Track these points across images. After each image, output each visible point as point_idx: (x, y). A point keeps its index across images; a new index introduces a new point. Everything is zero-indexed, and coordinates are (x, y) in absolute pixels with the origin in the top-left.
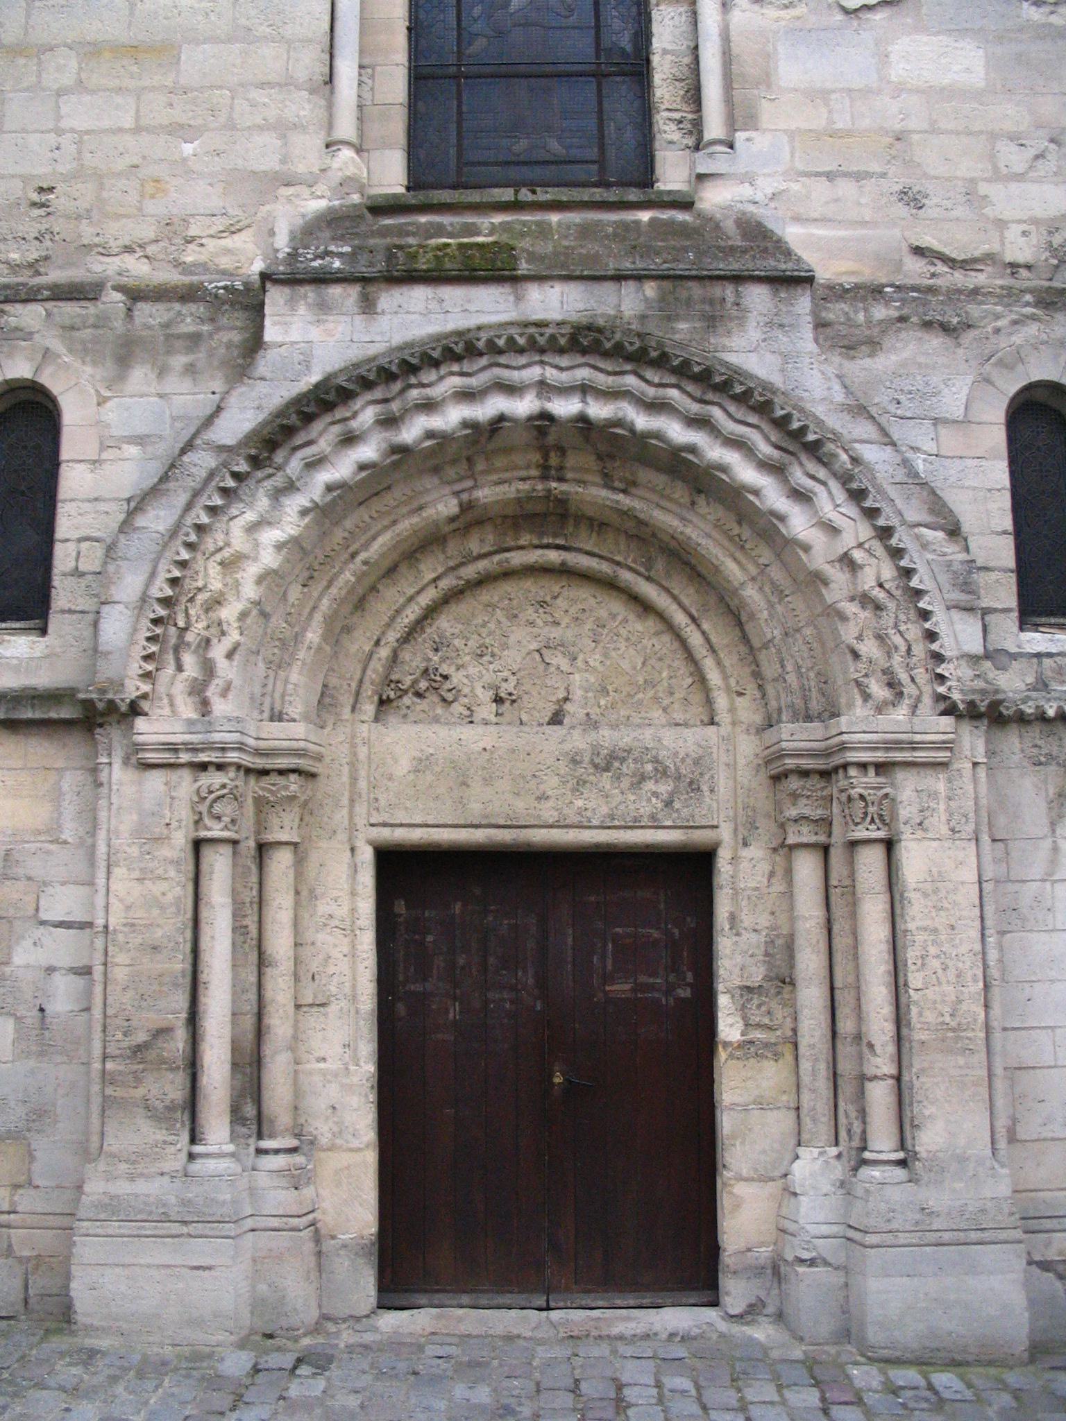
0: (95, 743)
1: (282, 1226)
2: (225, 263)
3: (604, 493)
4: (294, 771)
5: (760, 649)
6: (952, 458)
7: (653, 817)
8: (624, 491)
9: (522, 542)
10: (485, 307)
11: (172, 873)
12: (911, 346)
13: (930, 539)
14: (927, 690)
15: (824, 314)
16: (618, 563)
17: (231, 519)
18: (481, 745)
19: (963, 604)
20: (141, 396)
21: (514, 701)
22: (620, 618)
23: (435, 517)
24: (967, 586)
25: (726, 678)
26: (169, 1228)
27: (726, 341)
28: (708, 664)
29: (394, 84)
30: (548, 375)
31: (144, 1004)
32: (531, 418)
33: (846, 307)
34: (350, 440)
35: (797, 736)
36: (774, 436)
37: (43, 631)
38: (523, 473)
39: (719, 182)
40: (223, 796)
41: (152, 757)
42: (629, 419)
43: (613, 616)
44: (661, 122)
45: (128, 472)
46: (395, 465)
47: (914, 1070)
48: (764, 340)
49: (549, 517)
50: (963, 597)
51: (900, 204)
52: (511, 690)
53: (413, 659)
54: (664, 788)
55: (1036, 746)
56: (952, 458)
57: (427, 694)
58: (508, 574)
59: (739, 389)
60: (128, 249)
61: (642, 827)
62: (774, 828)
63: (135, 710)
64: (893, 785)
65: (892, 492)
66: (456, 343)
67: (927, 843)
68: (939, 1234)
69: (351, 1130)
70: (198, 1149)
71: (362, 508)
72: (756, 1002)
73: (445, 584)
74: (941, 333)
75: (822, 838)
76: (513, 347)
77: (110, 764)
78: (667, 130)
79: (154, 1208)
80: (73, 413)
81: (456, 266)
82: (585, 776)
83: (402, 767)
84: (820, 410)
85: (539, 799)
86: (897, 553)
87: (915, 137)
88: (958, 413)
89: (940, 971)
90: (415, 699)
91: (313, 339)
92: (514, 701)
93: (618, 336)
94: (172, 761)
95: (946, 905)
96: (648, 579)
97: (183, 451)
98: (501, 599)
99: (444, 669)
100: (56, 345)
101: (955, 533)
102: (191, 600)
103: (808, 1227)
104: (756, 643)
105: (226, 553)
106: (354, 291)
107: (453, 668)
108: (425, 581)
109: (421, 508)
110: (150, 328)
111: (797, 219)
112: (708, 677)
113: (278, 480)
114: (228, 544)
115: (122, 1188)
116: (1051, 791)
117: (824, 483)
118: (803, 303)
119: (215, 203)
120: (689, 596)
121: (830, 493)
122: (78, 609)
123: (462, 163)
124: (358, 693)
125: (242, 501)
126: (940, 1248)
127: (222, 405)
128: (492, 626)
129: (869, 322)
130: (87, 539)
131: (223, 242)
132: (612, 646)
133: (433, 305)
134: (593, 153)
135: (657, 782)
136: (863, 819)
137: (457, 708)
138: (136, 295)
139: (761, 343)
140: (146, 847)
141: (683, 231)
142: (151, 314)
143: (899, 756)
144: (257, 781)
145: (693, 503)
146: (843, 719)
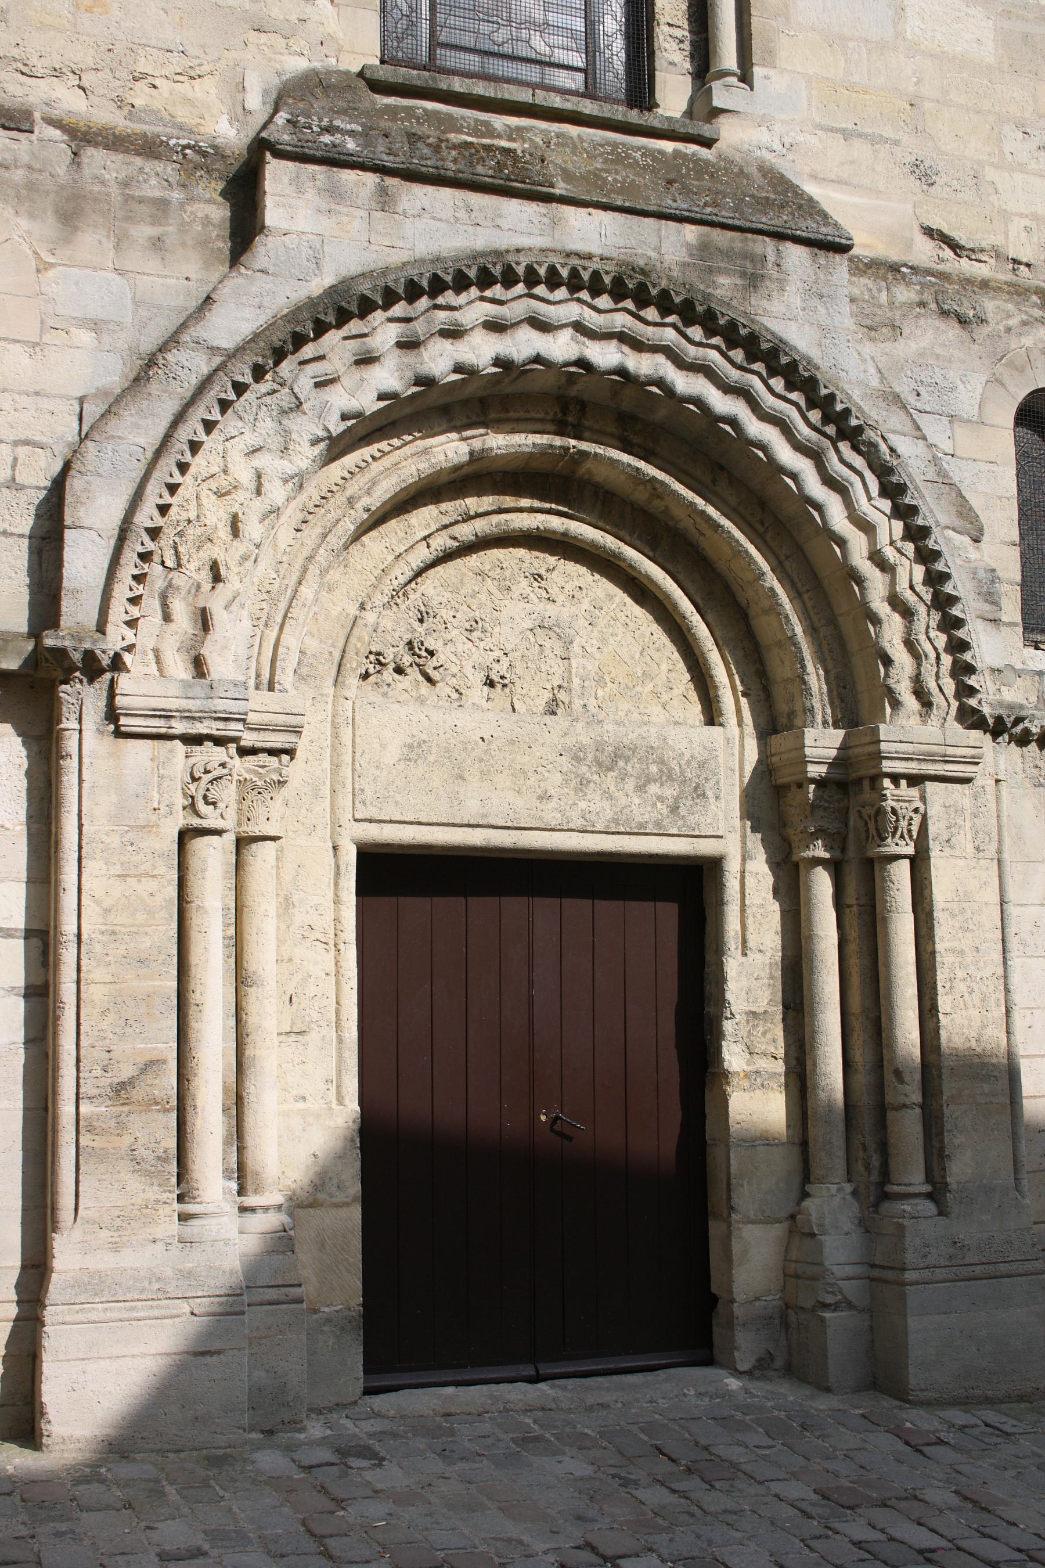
1: (283, 1298)
2: (184, 115)
6: (967, 459)
7: (658, 824)
10: (515, 226)
11: (162, 870)
13: (957, 543)
20: (95, 269)
21: (504, 686)
26: (168, 1307)
27: (765, 304)
30: (586, 316)
31: (128, 1030)
33: (870, 283)
34: (366, 360)
44: (661, 38)
47: (945, 1098)
50: (987, 607)
51: (912, 178)
53: (393, 628)
54: (670, 792)
56: (967, 459)
57: (409, 670)
59: (784, 360)
60: (57, 73)
67: (952, 860)
68: (971, 1268)
69: (335, 1182)
70: (190, 1208)
72: (761, 1029)
74: (957, 325)
76: (553, 281)
79: (146, 1284)
81: (490, 172)
82: (588, 775)
83: (393, 752)
84: (856, 394)
85: (540, 798)
89: (966, 995)
90: (396, 676)
91: (322, 228)
92: (504, 686)
93: (664, 283)
94: (163, 731)
103: (835, 1269)
106: (370, 179)
107: (440, 643)
111: (814, 177)
115: (104, 1261)
122: (16, 531)
126: (972, 1282)
127: (214, 296)
128: (483, 597)
130: (27, 443)
132: (611, 630)
133: (462, 214)
135: (662, 785)
138: (81, 137)
139: (799, 307)
140: (129, 836)
141: (701, 167)
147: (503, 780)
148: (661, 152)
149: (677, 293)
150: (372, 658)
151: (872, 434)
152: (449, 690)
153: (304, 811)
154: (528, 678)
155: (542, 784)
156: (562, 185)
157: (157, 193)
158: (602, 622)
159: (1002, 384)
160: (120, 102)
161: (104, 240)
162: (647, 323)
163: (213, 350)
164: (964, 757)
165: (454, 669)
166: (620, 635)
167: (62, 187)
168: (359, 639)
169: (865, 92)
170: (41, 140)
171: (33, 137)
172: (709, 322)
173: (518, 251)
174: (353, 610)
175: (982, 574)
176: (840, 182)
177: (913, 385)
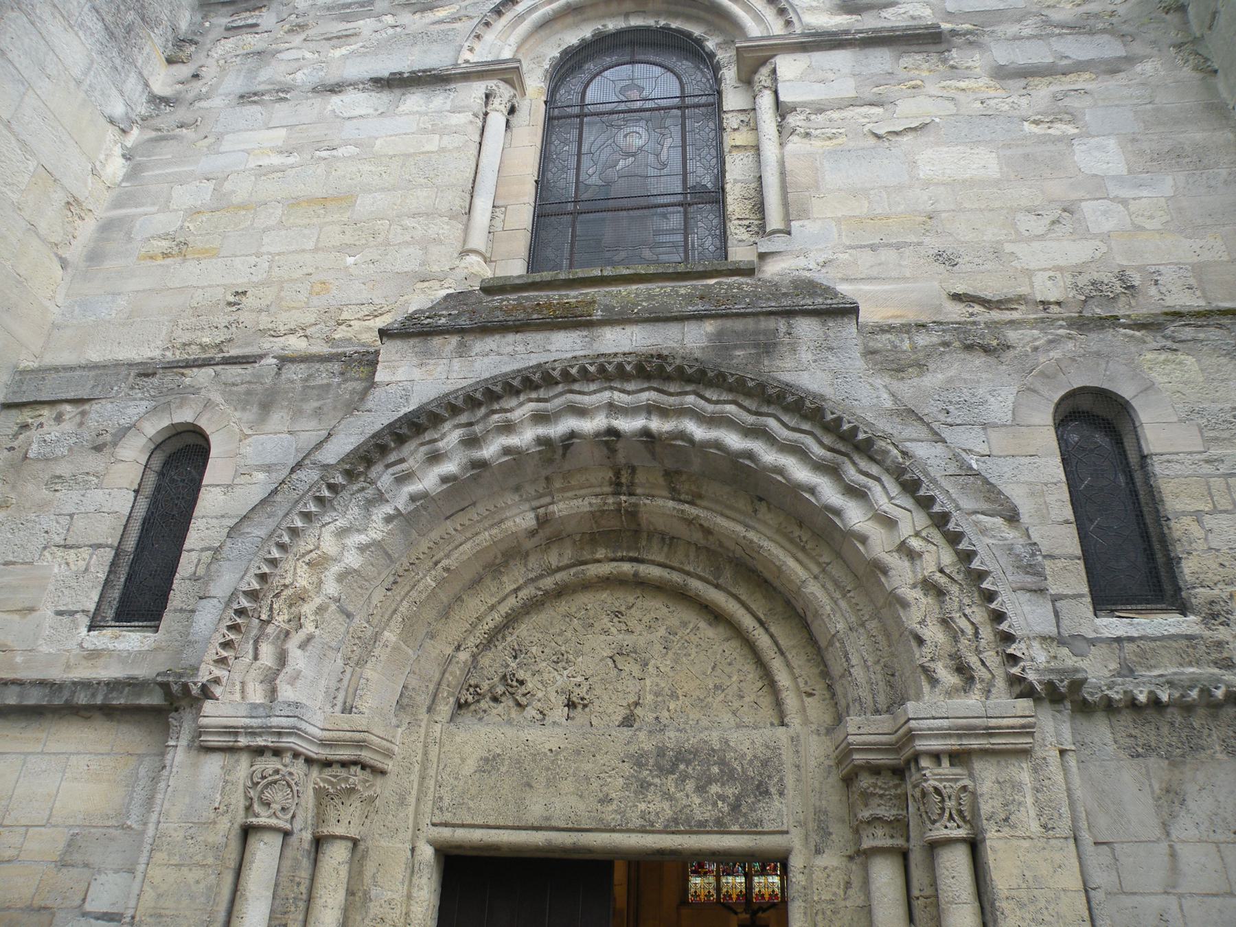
3: (671, 504)
4: (355, 763)
7: (719, 822)
8: (691, 503)
9: (599, 556)
10: (564, 346)
13: (988, 526)
14: (1000, 673)
15: (871, 344)
16: (688, 573)
17: (323, 526)
18: (548, 746)
23: (514, 529)
24: (1032, 569)
27: (778, 363)
28: (777, 664)
32: (597, 434)
34: (435, 458)
35: (865, 729)
36: (827, 440)
38: (598, 490)
39: (777, 258)
40: (275, 782)
41: (214, 740)
42: (688, 431)
43: (684, 624)
46: (474, 478)
48: (815, 361)
49: (622, 531)
50: (1029, 579)
52: (583, 694)
53: (494, 663)
54: (731, 791)
55: (1131, 736)
57: (503, 699)
58: (586, 586)
59: (790, 399)
60: (292, 332)
61: (708, 833)
62: (849, 835)
63: (206, 693)
64: (971, 776)
65: (945, 483)
67: (1015, 842)
71: (448, 522)
75: (899, 842)
76: (585, 375)
78: (737, 232)
82: (649, 778)
83: (471, 765)
84: (870, 417)
85: (601, 801)
86: (954, 539)
87: (944, 215)
90: (492, 704)
91: (412, 379)
92: (585, 706)
93: (678, 362)
95: (1047, 918)
96: (717, 586)
99: (521, 675)
100: (217, 397)
101: (1012, 517)
106: (454, 340)
107: (529, 673)
108: (507, 591)
109: (502, 521)
110: (292, 382)
111: (846, 280)
112: (777, 678)
113: (370, 493)
114: (318, 548)
116: (1156, 787)
117: (878, 479)
119: (364, 296)
120: (760, 606)
121: (884, 487)
124: (435, 695)
125: (335, 510)
128: (568, 634)
129: (914, 349)
131: (367, 323)
135: (723, 784)
136: (941, 815)
137: (531, 712)
139: (812, 364)
142: (295, 373)
143: (975, 743)
145: (755, 511)
146: (910, 705)
147: (567, 786)
149: (690, 367)
151: (883, 444)
152: (534, 713)
153: (390, 817)
154: (606, 698)
157: (325, 381)
158: (676, 647)
159: (1034, 391)
162: (671, 394)
164: (1012, 728)
165: (540, 695)
167: (267, 390)
168: (451, 674)
169: (888, 218)
174: (449, 650)
177: (941, 405)
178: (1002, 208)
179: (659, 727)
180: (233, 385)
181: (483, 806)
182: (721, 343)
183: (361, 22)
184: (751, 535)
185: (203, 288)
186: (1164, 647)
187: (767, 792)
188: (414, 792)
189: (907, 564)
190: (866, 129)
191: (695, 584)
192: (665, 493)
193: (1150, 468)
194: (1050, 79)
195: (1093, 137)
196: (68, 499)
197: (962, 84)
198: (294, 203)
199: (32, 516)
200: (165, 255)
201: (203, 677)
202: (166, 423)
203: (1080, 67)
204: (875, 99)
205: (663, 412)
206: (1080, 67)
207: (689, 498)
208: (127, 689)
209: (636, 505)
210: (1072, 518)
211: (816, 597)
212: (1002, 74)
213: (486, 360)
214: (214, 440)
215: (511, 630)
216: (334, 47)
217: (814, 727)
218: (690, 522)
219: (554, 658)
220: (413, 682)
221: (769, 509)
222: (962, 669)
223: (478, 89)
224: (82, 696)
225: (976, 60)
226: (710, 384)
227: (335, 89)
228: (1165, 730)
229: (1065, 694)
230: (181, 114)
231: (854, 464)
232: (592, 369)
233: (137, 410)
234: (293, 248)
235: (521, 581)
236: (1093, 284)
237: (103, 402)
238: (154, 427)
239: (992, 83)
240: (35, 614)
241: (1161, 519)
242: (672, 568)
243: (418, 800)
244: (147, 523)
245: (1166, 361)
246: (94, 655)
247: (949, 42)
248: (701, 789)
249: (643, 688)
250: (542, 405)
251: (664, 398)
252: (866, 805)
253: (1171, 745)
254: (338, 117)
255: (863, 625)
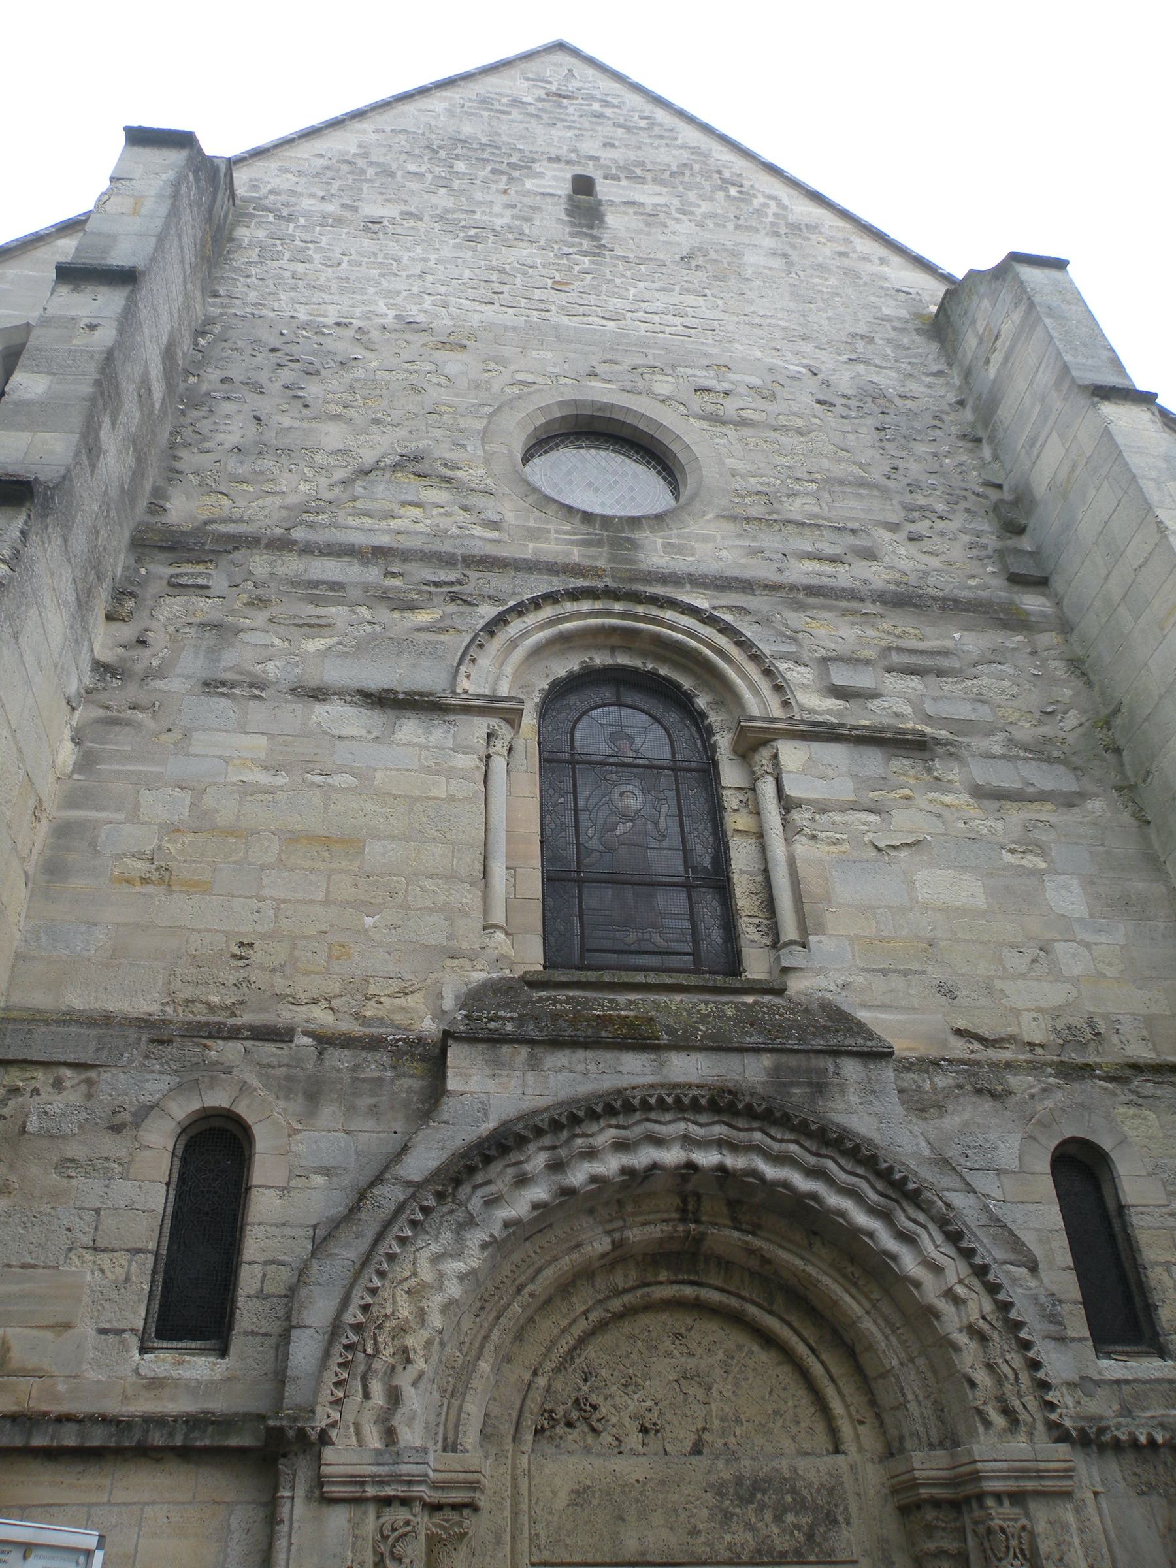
0: (276, 1475)
2: (399, 1018)
3: (736, 1234)
5: (876, 1379)
7: (797, 1552)
8: (753, 1234)
10: (633, 1070)
12: (969, 1110)
13: (1016, 1275)
16: (743, 1298)
18: (635, 1476)
19: (1054, 1334)
20: (329, 1131)
22: (746, 1349)
23: (591, 1254)
25: (847, 1406)
27: (830, 1104)
28: (830, 1392)
29: (533, 884)
32: (678, 1167)
34: (522, 1181)
35: (928, 1465)
36: (880, 1186)
37: (223, 1352)
38: (665, 1216)
39: (799, 974)
40: (406, 1535)
43: (740, 1347)
45: (319, 1199)
46: (561, 1204)
50: (1052, 1327)
53: (567, 1386)
54: (804, 1520)
55: (1135, 1474)
57: (578, 1424)
58: (648, 1307)
59: (850, 1145)
60: (315, 1001)
64: (1027, 1515)
66: (616, 1100)
71: (527, 1243)
73: (594, 1316)
74: (990, 1099)
76: (662, 1105)
77: (293, 1498)
78: (750, 933)
80: (264, 1142)
82: (731, 1509)
83: (563, 1499)
84: (912, 1164)
86: (993, 1289)
87: (942, 944)
88: (1014, 1165)
90: (567, 1430)
91: (488, 1091)
92: (657, 1431)
93: (747, 1099)
96: (771, 1312)
97: (372, 1185)
98: (642, 1331)
99: (594, 1399)
100: (254, 1082)
102: (379, 1327)
104: (871, 1373)
105: (412, 1282)
106: (524, 1051)
107: (601, 1398)
109: (578, 1246)
110: (339, 1070)
111: (864, 1006)
112: (831, 1405)
113: (460, 1215)
116: (1160, 1524)
117: (924, 1227)
118: (887, 1074)
123: (584, 950)
125: (427, 1233)
128: (635, 1356)
129: (934, 1089)
130: (273, 1262)
134: (688, 948)
135: (797, 1514)
137: (606, 1438)
138: (325, 1041)
139: (863, 1107)
141: (773, 1010)
142: (339, 1059)
143: (1030, 1485)
144: (430, 1516)
145: (810, 1244)
147: (657, 1518)
148: (744, 1004)
149: (759, 1105)
150: (546, 1415)
151: (928, 1194)
152: (610, 1439)
153: (488, 1558)
154: (676, 1423)
155: (692, 1520)
156: (666, 1037)
157: (376, 1074)
160: (357, 1016)
161: (337, 1110)
163: (408, 1183)
165: (614, 1420)
166: (751, 1380)
167: (310, 1077)
168: (533, 1400)
170: (298, 1046)
171: (293, 1045)
172: (785, 1121)
173: (634, 1088)
174: (527, 1376)
175: (1043, 1299)
176: (883, 1007)
178: (990, 941)
179: (733, 1458)
180: (269, 1066)
181: (580, 1543)
182: (780, 1079)
183: (333, 609)
184: (810, 1269)
185: (199, 931)
186: (1152, 1390)
187: (835, 1521)
188: (508, 1530)
189: (953, 1309)
190: (866, 839)
191: (752, 1310)
192: (728, 1222)
193: (1127, 1218)
194: (1020, 804)
195: (1059, 874)
196: (90, 1190)
197: (947, 799)
198: (292, 838)
199: (46, 1208)
200: (144, 881)
201: (321, 1421)
202: (196, 1106)
203: (1043, 796)
204: (872, 805)
205: (734, 1147)
206: (1043, 796)
207: (749, 1228)
208: (210, 1428)
209: (704, 1234)
210: (1072, 1265)
211: (871, 1333)
212: (980, 793)
213: (560, 1077)
214: (258, 1131)
215: (578, 1351)
216: (306, 637)
217: (869, 1455)
218: (751, 1251)
219: (623, 1381)
220: (495, 1410)
221: (823, 1244)
222: (1007, 1411)
223: (479, 726)
224: (157, 1435)
225: (953, 773)
226: (775, 1123)
227: (319, 694)
228: (1161, 1469)
229: (1090, 1440)
230: (133, 691)
231: (904, 1210)
232: (670, 1100)
233: (157, 1086)
234: (300, 895)
235: (590, 1303)
236: (1068, 1028)
237: (114, 1070)
238: (182, 1109)
239: (972, 801)
240: (72, 1331)
241: (1138, 1267)
242: (728, 1292)
243: (513, 1537)
244: (175, 1215)
245: (1134, 1116)
246: (156, 1384)
247: (932, 750)
248: (778, 1519)
249: (709, 1413)
250: (622, 1132)
251: (734, 1133)
252: (930, 1537)
253: (1166, 1484)
254: (325, 733)
255: (912, 1360)
